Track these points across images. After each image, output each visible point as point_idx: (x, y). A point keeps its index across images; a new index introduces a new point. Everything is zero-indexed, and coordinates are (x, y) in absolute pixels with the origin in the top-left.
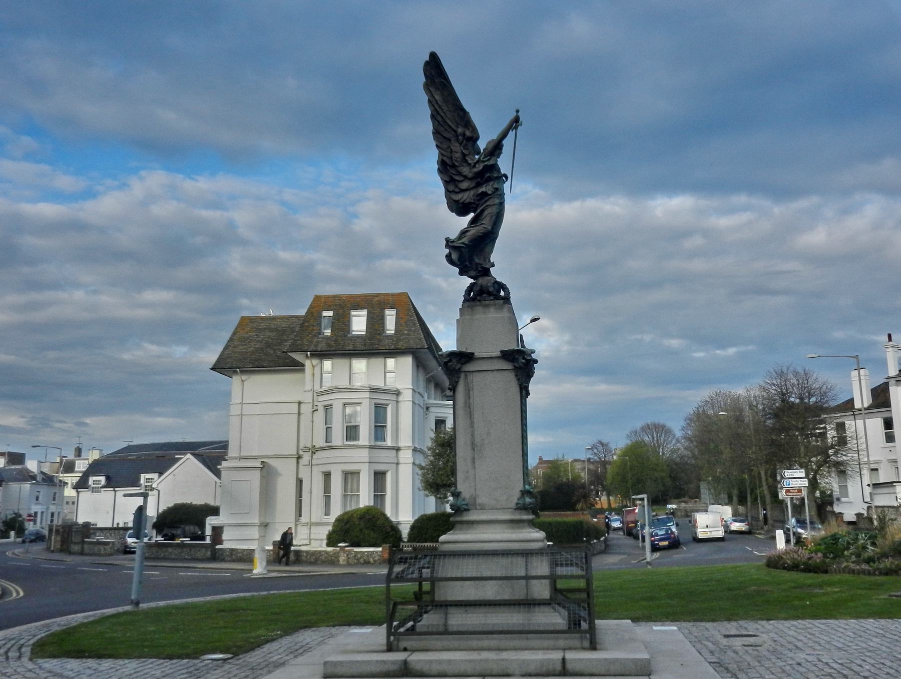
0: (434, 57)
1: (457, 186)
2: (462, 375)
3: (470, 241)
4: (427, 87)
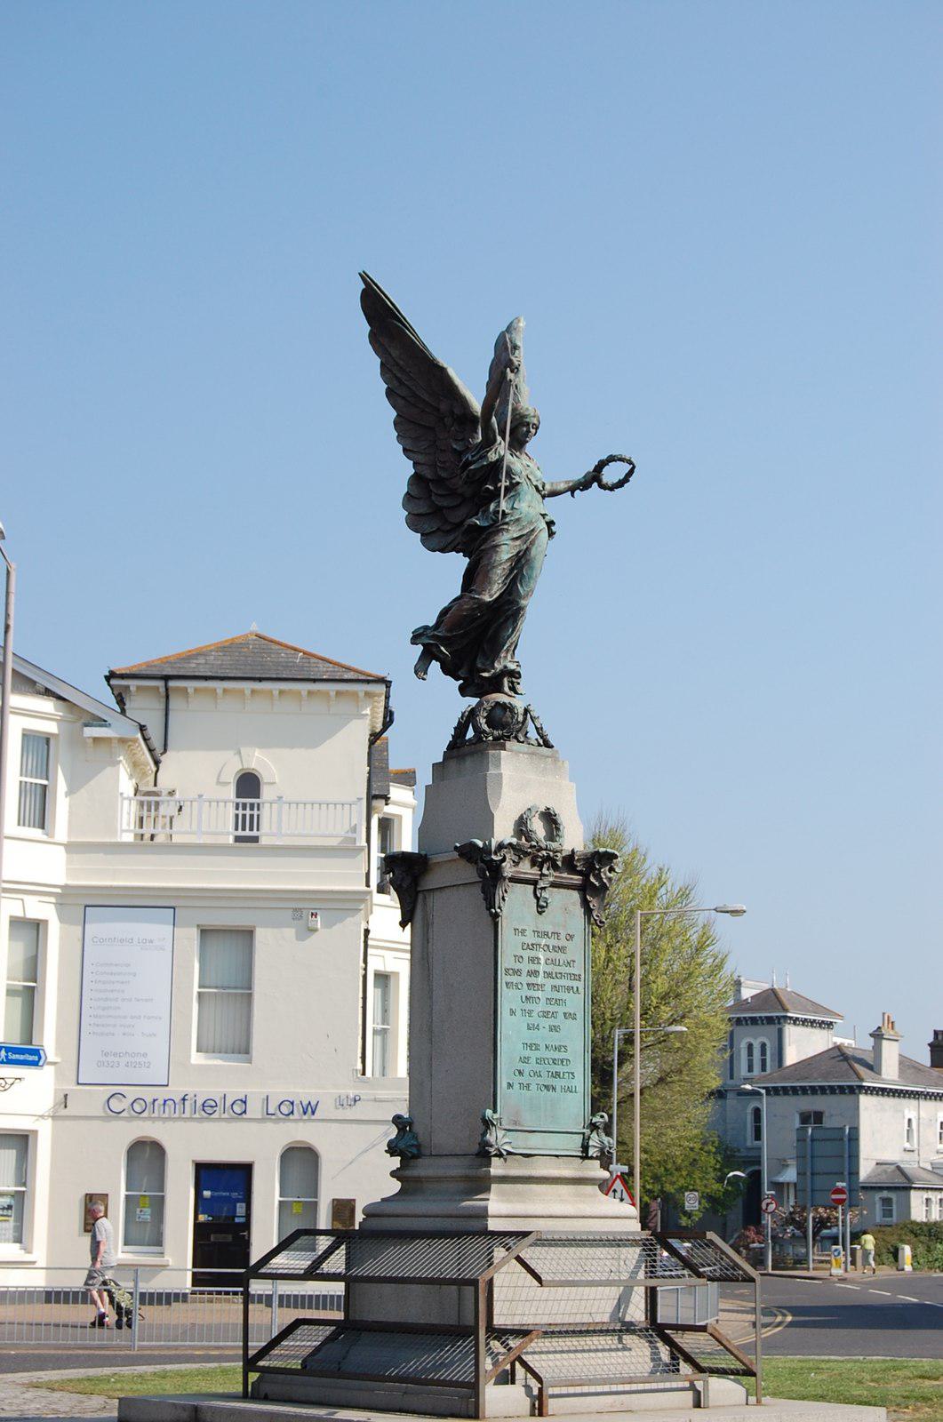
0: (365, 277)
1: (446, 521)
2: (421, 896)
3: (450, 630)
4: (374, 338)
